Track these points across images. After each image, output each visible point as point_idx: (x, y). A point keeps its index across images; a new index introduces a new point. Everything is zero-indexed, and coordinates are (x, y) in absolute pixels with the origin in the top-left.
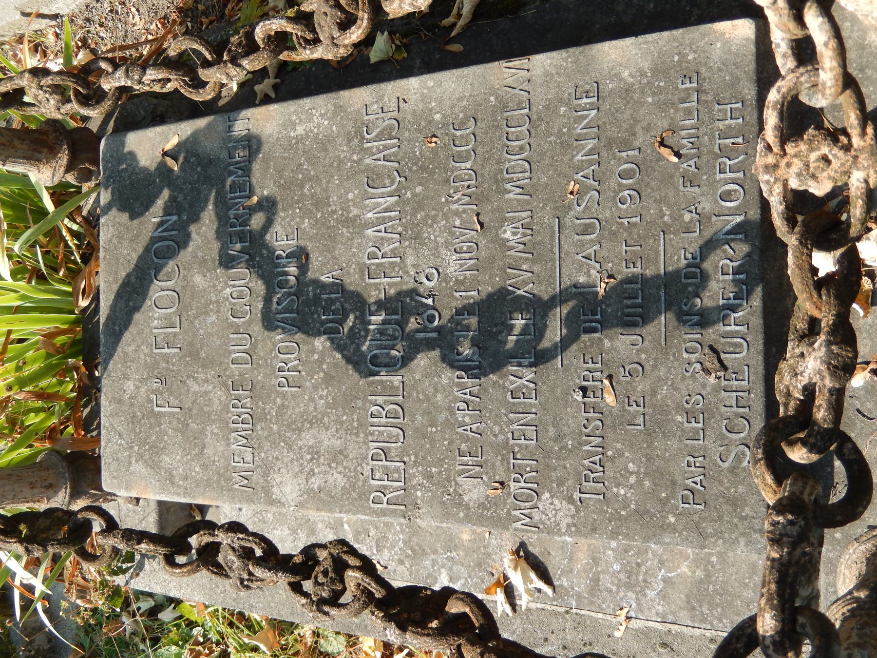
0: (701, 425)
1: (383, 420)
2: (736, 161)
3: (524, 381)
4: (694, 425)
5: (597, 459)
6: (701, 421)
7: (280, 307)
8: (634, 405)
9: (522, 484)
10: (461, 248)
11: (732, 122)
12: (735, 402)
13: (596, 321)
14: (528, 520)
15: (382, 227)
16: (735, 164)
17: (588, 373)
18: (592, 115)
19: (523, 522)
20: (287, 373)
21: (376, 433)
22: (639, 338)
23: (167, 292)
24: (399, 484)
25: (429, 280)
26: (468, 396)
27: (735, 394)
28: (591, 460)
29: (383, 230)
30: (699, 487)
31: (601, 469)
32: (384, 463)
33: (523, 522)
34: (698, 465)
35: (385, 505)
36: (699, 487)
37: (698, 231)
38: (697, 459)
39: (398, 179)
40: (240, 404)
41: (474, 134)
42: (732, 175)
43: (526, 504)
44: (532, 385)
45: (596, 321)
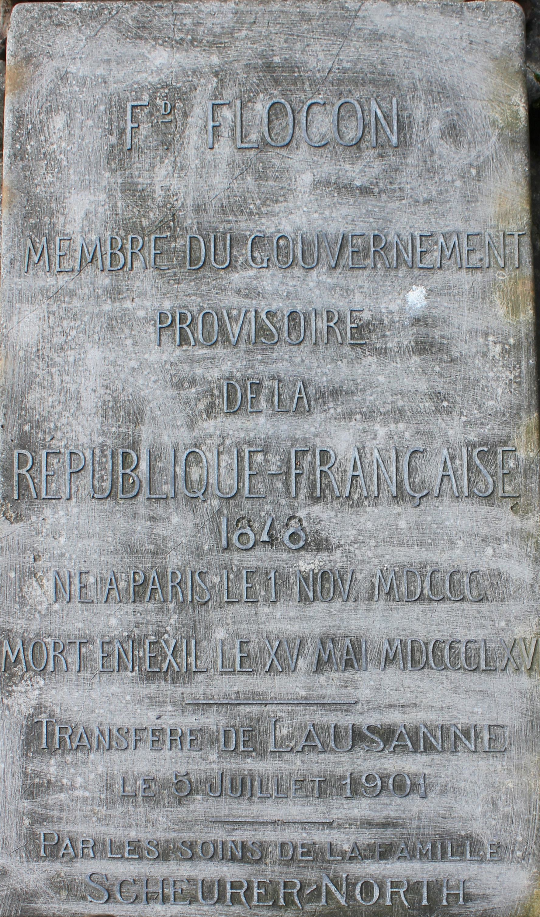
0: (126, 855)
1: (120, 471)
2: (403, 898)
3: (170, 657)
4: (127, 849)
5: (85, 741)
6: (130, 857)
7: (263, 316)
8: (145, 786)
9: (52, 653)
10: (328, 580)
11: (445, 895)
12: (151, 890)
13: (237, 746)
14: (13, 659)
15: (359, 472)
16: (400, 896)
17: (180, 734)
18: (469, 746)
19: (389, 650)
20: (178, 326)
21: (104, 460)
22: (219, 794)
23: (302, 336)
24: (44, 490)
25: (291, 536)
26: (150, 587)
27: (161, 891)
28: (84, 736)
29: (356, 473)
30: (62, 851)
31: (74, 747)
32: (69, 470)
33: (389, 650)
34: (86, 851)
35: (16, 471)
36: (62, 851)
37: (332, 858)
38: (91, 850)
39: (418, 495)
40: (136, 251)
41: (462, 599)
42: (388, 895)
43: (30, 657)
44: (165, 667)
45: (237, 746)
